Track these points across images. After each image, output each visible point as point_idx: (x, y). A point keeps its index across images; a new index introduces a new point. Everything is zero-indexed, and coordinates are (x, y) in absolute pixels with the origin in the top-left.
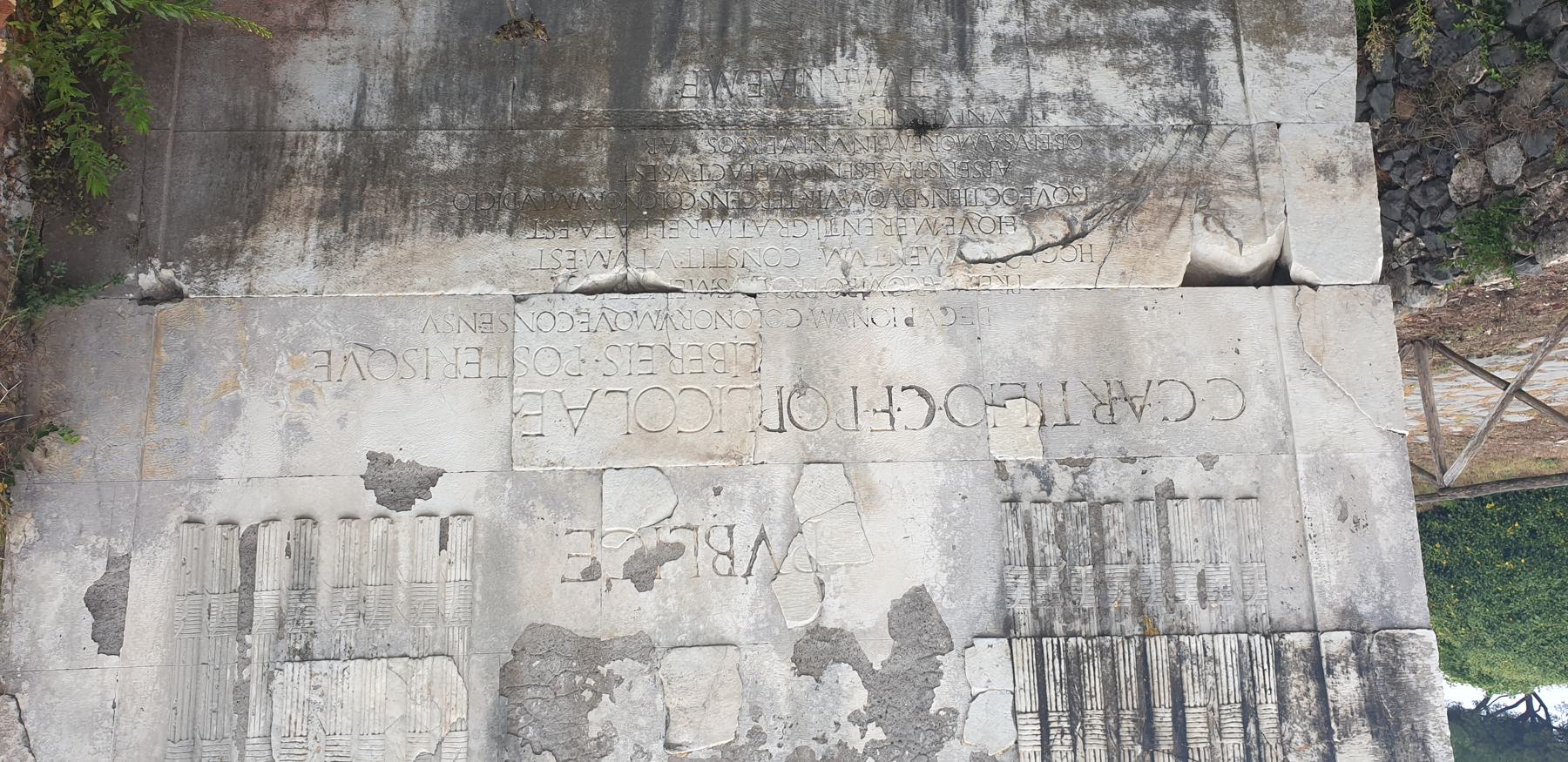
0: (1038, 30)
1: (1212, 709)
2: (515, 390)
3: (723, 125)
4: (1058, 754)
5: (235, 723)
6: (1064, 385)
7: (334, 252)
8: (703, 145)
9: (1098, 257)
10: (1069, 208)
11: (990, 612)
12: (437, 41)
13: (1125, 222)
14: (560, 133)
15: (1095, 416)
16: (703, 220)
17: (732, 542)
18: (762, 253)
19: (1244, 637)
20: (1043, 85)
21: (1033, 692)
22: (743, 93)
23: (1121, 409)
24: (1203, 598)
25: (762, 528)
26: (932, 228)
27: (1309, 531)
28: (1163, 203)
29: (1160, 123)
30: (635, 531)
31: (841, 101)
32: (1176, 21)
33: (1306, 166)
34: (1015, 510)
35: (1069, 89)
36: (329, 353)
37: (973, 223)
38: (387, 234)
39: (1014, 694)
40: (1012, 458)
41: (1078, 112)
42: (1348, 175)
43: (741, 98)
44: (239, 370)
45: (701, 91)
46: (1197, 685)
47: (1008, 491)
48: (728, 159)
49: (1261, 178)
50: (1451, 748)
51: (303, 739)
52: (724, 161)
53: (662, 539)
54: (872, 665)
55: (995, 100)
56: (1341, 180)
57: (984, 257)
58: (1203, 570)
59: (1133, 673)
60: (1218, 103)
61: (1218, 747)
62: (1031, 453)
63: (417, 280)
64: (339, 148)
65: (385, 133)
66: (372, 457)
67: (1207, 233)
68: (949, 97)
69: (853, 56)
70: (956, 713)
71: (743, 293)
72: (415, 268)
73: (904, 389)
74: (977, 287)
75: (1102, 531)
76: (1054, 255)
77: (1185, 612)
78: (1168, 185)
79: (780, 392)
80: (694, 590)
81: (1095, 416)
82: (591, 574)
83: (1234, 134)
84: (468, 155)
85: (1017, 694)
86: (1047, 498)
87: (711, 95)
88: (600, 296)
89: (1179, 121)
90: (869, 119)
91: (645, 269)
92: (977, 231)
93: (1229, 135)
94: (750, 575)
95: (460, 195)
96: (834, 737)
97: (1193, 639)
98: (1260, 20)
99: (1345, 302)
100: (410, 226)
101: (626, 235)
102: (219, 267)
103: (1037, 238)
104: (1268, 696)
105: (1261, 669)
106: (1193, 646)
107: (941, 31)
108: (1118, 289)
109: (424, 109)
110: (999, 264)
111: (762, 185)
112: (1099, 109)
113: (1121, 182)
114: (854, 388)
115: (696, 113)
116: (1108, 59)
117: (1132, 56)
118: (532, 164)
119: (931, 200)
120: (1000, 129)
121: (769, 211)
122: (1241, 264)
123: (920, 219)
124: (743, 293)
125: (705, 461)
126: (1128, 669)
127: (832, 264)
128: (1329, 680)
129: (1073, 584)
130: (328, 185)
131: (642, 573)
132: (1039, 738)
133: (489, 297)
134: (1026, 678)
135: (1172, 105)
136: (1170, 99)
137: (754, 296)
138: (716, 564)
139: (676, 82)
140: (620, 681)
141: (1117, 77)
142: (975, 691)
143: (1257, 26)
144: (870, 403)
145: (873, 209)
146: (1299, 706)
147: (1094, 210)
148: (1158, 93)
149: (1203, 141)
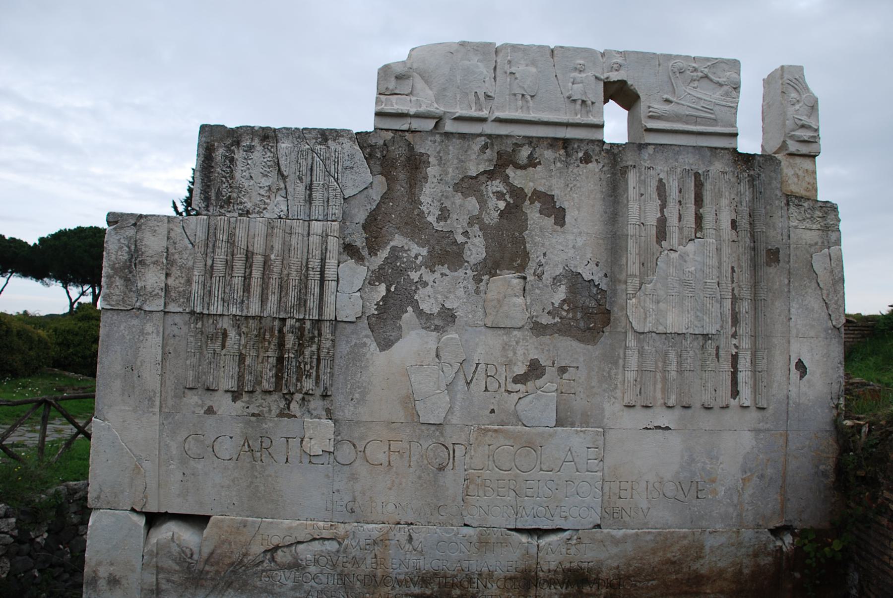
1: (229, 275)
2: (601, 474)
4: (317, 258)
5: (737, 306)
6: (287, 461)
10: (272, 569)
13: (240, 558)
16: (493, 572)
17: (486, 382)
18: (459, 551)
19: (206, 312)
23: (256, 446)
24: (225, 334)
27: (159, 367)
30: (539, 392)
33: (126, 585)
34: (324, 391)
37: (330, 563)
39: (337, 291)
42: (101, 578)
44: (742, 489)
46: (236, 288)
49: (154, 580)
50: (105, 245)
51: (706, 295)
53: (524, 386)
54: (413, 311)
56: (106, 575)
57: (326, 542)
58: (222, 350)
61: (229, 255)
62: (311, 422)
63: (653, 538)
67: (192, 547)
70: (369, 283)
71: (472, 526)
72: (653, 545)
75: (277, 376)
76: (284, 540)
77: (236, 328)
78: (213, 579)
80: (508, 357)
82: (563, 370)
85: (335, 291)
88: (554, 527)
91: (528, 543)
92: (329, 558)
94: (477, 364)
95: (629, 588)
97: (234, 313)
99: (116, 499)
103: (294, 551)
105: (199, 294)
106: (235, 309)
108: (248, 517)
110: (318, 537)
119: (355, 578)
122: (173, 527)
123: (363, 567)
124: (472, 526)
125: (499, 429)
126: (273, 299)
127: (417, 542)
131: (535, 370)
133: (614, 527)
134: (329, 298)
137: (465, 525)
138: (495, 371)
140: (549, 313)
142: (358, 294)
145: (391, 575)
147: (257, 567)
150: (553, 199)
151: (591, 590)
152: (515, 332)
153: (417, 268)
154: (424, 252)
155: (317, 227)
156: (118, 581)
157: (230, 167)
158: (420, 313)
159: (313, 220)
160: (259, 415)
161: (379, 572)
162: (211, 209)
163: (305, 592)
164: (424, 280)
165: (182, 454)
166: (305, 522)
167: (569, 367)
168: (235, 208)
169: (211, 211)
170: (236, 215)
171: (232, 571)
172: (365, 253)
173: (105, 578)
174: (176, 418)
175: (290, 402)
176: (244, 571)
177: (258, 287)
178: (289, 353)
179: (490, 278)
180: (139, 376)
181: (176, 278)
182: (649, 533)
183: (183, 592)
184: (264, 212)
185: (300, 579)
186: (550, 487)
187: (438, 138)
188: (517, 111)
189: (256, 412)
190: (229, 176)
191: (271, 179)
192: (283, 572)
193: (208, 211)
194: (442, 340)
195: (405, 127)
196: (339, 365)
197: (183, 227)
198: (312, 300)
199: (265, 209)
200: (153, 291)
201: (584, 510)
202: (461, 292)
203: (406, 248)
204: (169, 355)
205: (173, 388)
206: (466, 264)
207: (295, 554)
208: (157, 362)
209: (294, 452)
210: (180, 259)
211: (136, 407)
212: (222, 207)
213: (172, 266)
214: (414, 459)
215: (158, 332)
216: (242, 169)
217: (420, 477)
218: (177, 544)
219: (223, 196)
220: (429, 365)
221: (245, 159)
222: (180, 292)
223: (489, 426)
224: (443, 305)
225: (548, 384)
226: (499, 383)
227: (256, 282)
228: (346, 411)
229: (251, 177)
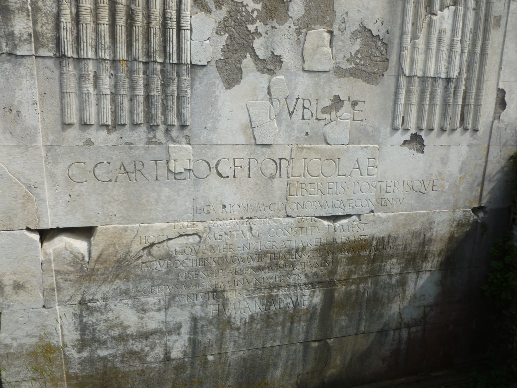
0: (160, 339)
3: (295, 286)
4: (173, 9)
6: (157, 179)
7: (429, 227)
8: (303, 277)
9: (138, 239)
11: (198, 76)
12: (391, 307)
13: (124, 256)
14: (354, 277)
15: (143, 164)
17: (303, 113)
20: (159, 315)
21: (183, 39)
22: (286, 299)
23: (130, 168)
25: (291, 118)
26: (212, 248)
28: (105, 265)
31: (248, 300)
32: (94, 351)
33: (30, 288)
35: (147, 314)
36: (433, 190)
37: (194, 251)
38: (412, 235)
40: (183, 145)
41: (143, 304)
42: (6, 285)
43: (287, 297)
45: (302, 298)
46: (103, 35)
47: (186, 132)
48: (294, 272)
52: (296, 271)
55: (182, 306)
56: (11, 282)
57: (190, 237)
59: (134, 43)
60: (75, 315)
62: (174, 148)
64: (424, 265)
65: (410, 271)
66: (423, 152)
69: (241, 319)
70: (217, 33)
73: (228, 177)
74: (194, 223)
78: (102, 274)
79: (280, 175)
81: (143, 164)
82: (355, 103)
83: (67, 300)
84: (385, 265)
86: (168, 127)
87: (299, 297)
89: (94, 304)
90: (237, 294)
91: (328, 225)
93: (69, 300)
96: (268, 27)
98: (51, 356)
100: (405, 238)
101: (334, 239)
102: (462, 220)
104: (65, 26)
106: (103, 54)
107: (204, 334)
109: (397, 281)
110: (183, 234)
111: (282, 262)
112: (133, 306)
113: (125, 273)
114: (249, 177)
115: (305, 289)
116: (129, 329)
117: (117, 332)
118: (364, 264)
119: (212, 260)
120: (180, 293)
121: (280, 252)
125: (311, 147)
126: (139, 46)
128: (31, 31)
129: (160, 87)
130: (428, 252)
131: (337, 102)
132: (182, 17)
133: (382, 212)
135: (97, 311)
136: (99, 314)
137: (288, 216)
139: (311, 301)
140: (348, 60)
141: (124, 322)
142: (208, 42)
143: (53, 353)
144: (243, 170)
145: (237, 256)
146: (47, 20)
147: (138, 260)
148: (104, 317)
149: (83, 296)
151: (366, 253)
153: (253, 22)
158: (255, 57)
161: (229, 254)
164: (258, 31)
166: (173, 224)
167: (359, 101)
173: (10, 285)
177: (123, 35)
179: (308, 31)
182: (402, 214)
186: (343, 187)
192: (159, 262)
198: (171, 46)
201: (364, 201)
207: (167, 248)
209: (162, 172)
218: (70, 252)
224: (273, 53)
225: (345, 112)
226: (312, 113)
228: (201, 138)
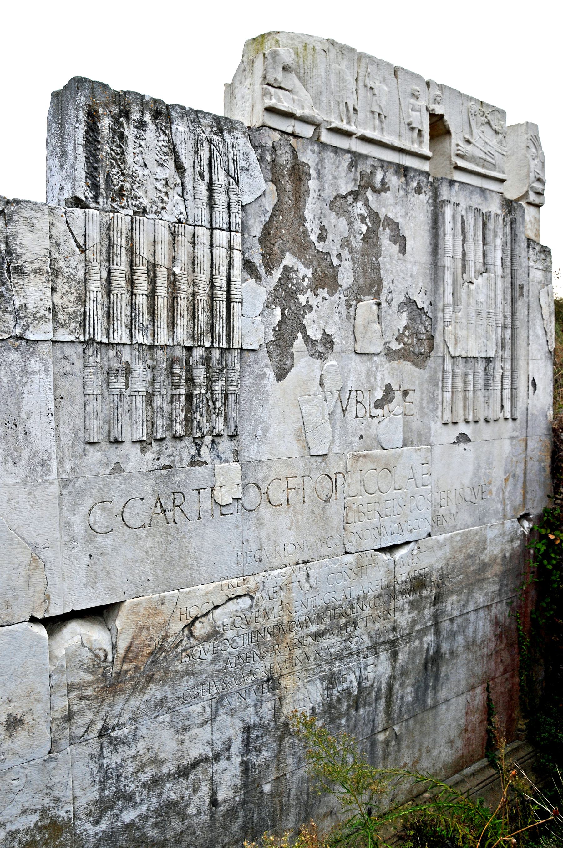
10: (192, 645)
24: (128, 371)
27: (52, 418)
29: (133, 727)
37: (245, 622)
57: (240, 600)
62: (221, 468)
68: (256, 705)
78: (132, 678)
82: (406, 393)
89: (120, 732)
92: (243, 616)
93: (86, 732)
97: (141, 341)
103: (211, 619)
106: (141, 336)
108: (164, 591)
110: (233, 596)
119: (266, 632)
126: (183, 322)
136: (126, 748)
145: (294, 619)
148: (133, 751)
150: (398, 226)
152: (376, 358)
154: (309, 273)
155: (221, 237)
156: (20, 721)
157: (120, 147)
158: (307, 338)
159: (216, 229)
160: (170, 467)
161: (285, 619)
162: (101, 200)
163: (224, 661)
165: (86, 531)
166: (220, 583)
168: (130, 203)
169: (101, 203)
170: (131, 213)
171: (153, 662)
172: (262, 271)
174: (77, 484)
175: (200, 447)
176: (165, 657)
178: (200, 388)
179: (357, 303)
180: (26, 434)
181: (64, 294)
183: (100, 706)
184: (163, 212)
185: (219, 648)
187: (316, 148)
188: (375, 130)
189: (168, 464)
190: (120, 159)
191: (167, 171)
193: (98, 203)
194: (325, 368)
195: (290, 130)
196: (244, 400)
197: (67, 222)
198: (221, 325)
199: (163, 208)
200: (37, 312)
202: (336, 318)
203: (295, 269)
204: (61, 400)
205: (70, 445)
206: (340, 288)
208: (49, 412)
209: (207, 504)
210: (67, 267)
211: (26, 476)
212: (113, 200)
213: (57, 277)
214: (307, 493)
215: (47, 370)
216: (134, 151)
217: (312, 512)
219: (114, 186)
220: (314, 394)
221: (137, 138)
222: (70, 314)
223: (360, 452)
224: (324, 331)
227: (162, 303)
228: (251, 451)
229: (145, 165)
